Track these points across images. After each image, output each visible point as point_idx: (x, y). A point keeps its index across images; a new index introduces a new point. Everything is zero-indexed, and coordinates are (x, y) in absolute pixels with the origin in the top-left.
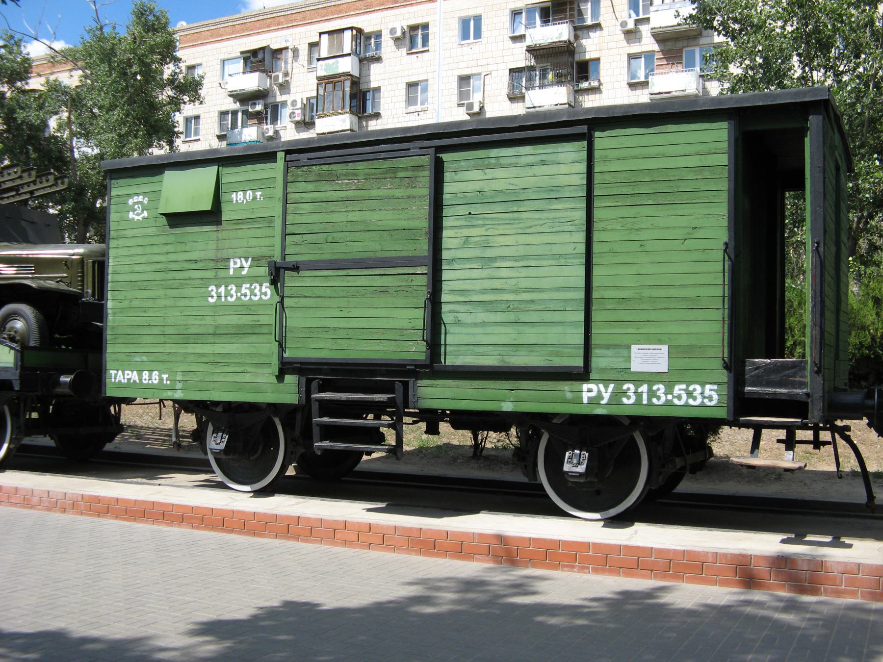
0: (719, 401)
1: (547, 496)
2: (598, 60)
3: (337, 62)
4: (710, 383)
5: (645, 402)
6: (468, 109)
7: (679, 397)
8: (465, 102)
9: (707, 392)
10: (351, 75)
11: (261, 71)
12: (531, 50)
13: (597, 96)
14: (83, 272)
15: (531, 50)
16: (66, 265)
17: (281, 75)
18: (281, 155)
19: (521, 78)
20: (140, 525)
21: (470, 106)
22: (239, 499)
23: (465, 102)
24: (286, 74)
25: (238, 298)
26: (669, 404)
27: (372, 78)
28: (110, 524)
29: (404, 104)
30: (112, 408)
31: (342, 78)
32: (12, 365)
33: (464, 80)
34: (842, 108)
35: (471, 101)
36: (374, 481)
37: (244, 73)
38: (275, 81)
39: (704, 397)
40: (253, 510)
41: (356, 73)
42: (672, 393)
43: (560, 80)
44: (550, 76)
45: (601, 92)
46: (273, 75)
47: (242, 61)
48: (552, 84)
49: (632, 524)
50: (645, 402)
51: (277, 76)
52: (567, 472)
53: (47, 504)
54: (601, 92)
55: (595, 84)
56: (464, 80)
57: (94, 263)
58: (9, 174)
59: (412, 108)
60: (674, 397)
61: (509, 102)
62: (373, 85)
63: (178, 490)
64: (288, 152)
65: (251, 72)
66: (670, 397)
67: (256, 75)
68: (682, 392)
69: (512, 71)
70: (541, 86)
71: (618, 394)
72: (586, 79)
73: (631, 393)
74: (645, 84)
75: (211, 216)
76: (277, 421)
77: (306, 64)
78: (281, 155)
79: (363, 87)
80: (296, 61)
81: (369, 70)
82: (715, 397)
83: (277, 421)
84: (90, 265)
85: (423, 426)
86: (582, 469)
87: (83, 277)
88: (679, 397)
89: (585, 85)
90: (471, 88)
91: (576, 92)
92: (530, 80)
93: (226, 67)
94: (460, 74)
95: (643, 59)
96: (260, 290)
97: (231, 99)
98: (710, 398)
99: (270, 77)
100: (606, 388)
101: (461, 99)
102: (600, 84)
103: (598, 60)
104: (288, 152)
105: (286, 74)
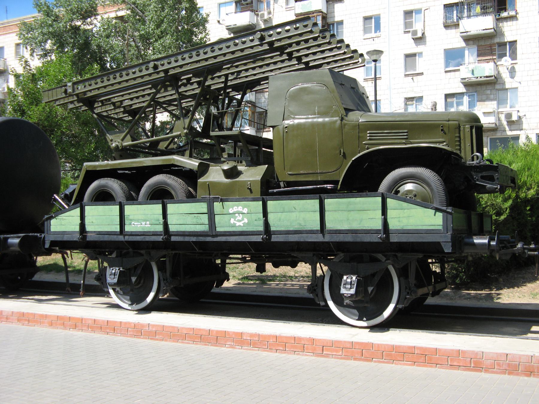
1: (330, 310)
2: (341, 23)
6: (413, 35)
8: (411, 30)
10: (322, 12)
11: (252, 11)
12: (229, 29)
13: (514, 22)
14: (460, 137)
15: (229, 29)
16: (442, 130)
17: (266, 14)
19: (453, 11)
20: (399, 367)
21: (415, 33)
22: (128, 316)
23: (411, 30)
24: (270, 13)
27: (336, 14)
28: (143, 342)
29: (362, 32)
31: (315, 14)
32: (441, 228)
33: (408, 14)
35: (414, 29)
36: (484, 316)
37: (236, 13)
38: (261, 17)
40: (435, 347)
41: (325, 11)
43: (485, 12)
44: (478, 9)
45: (517, 19)
46: (260, 13)
47: (234, 4)
48: (477, 15)
49: (150, 313)
51: (263, 15)
52: (343, 294)
53: (505, 367)
54: (517, 19)
55: (512, 13)
56: (408, 14)
57: (472, 128)
58: (90, 85)
59: (368, 36)
61: (444, 29)
62: (337, 19)
63: (86, 308)
65: (241, 12)
67: (248, 13)
69: (446, 6)
70: (469, 17)
72: (505, 10)
74: (457, 26)
75: (409, 100)
77: (284, 4)
79: (329, 21)
80: (277, 3)
81: (334, 8)
84: (469, 130)
85: (254, 265)
86: (353, 291)
87: (460, 141)
89: (504, 14)
90: (414, 20)
91: (497, 20)
92: (462, 12)
93: (221, 8)
94: (405, 9)
95: (373, 20)
97: (227, 31)
99: (257, 15)
101: (406, 28)
102: (517, 13)
103: (341, 23)
105: (270, 13)
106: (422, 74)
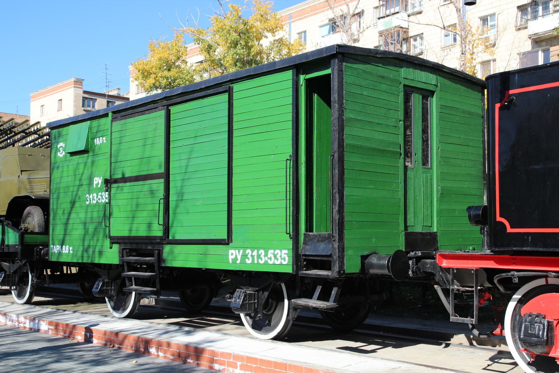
0: (288, 262)
3: (391, 19)
4: (284, 249)
5: (256, 262)
7: (270, 259)
9: (283, 256)
18: (110, 114)
25: (97, 201)
26: (266, 263)
30: (49, 273)
34: (462, 68)
39: (282, 259)
42: (267, 256)
50: (256, 262)
60: (268, 258)
64: (114, 113)
66: (266, 258)
68: (286, 255)
71: (245, 256)
73: (249, 256)
76: (283, 285)
78: (110, 114)
82: (287, 259)
83: (283, 285)
88: (270, 259)
96: (97, 197)
98: (284, 259)
100: (239, 252)
104: (114, 113)
106: (420, 13)
